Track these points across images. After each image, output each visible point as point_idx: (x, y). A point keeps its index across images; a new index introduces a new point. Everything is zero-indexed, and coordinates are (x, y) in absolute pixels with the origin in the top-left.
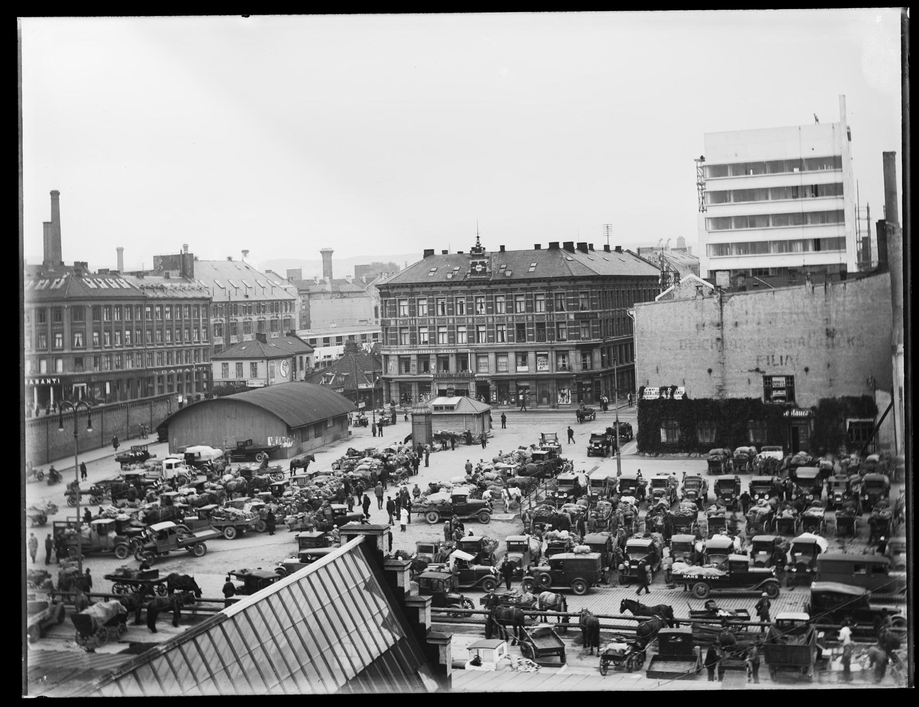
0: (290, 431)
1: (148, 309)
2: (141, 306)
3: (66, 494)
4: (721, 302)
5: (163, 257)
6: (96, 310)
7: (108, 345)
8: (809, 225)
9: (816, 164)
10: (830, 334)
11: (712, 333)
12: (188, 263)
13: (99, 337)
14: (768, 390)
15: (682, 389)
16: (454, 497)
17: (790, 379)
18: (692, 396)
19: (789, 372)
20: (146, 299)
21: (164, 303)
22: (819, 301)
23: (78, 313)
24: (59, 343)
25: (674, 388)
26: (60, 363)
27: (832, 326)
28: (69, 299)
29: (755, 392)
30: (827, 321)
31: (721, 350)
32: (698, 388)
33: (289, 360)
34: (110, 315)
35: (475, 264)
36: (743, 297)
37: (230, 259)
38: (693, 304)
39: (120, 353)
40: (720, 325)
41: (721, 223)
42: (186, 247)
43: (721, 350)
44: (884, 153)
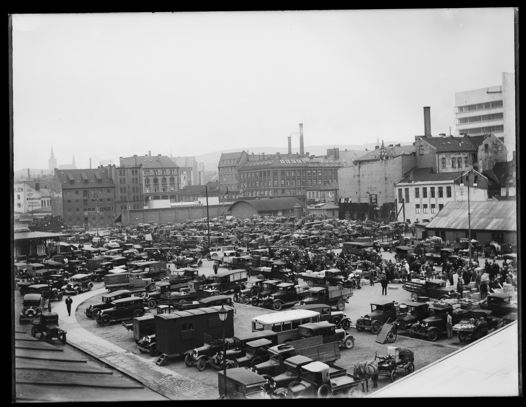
0: (260, 212)
2: (305, 170)
4: (359, 167)
5: (330, 150)
6: (283, 173)
7: (289, 185)
9: (487, 105)
10: (386, 179)
11: (357, 179)
12: (337, 152)
13: (284, 182)
14: (371, 200)
15: (350, 199)
16: (215, 225)
17: (376, 195)
18: (352, 202)
20: (307, 167)
21: (317, 169)
22: (383, 166)
25: (348, 199)
26: (270, 192)
27: (387, 176)
28: (272, 168)
31: (359, 185)
32: (353, 200)
33: (334, 192)
34: (290, 174)
35: (381, 152)
37: (366, 150)
38: (352, 168)
40: (359, 176)
42: (150, 152)
43: (359, 185)
44: (425, 108)
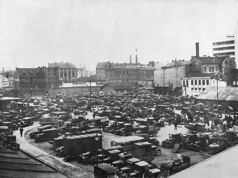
1: (140, 72)
3: (179, 114)
4: (164, 70)
8: (217, 50)
10: (177, 76)
15: (159, 85)
17: (172, 83)
19: (172, 82)
23: (124, 72)
24: (121, 77)
27: (178, 74)
29: (168, 86)
30: (177, 73)
31: (164, 78)
33: (152, 81)
36: (172, 69)
38: (161, 70)
39: (133, 79)
40: (164, 74)
41: (215, 49)
